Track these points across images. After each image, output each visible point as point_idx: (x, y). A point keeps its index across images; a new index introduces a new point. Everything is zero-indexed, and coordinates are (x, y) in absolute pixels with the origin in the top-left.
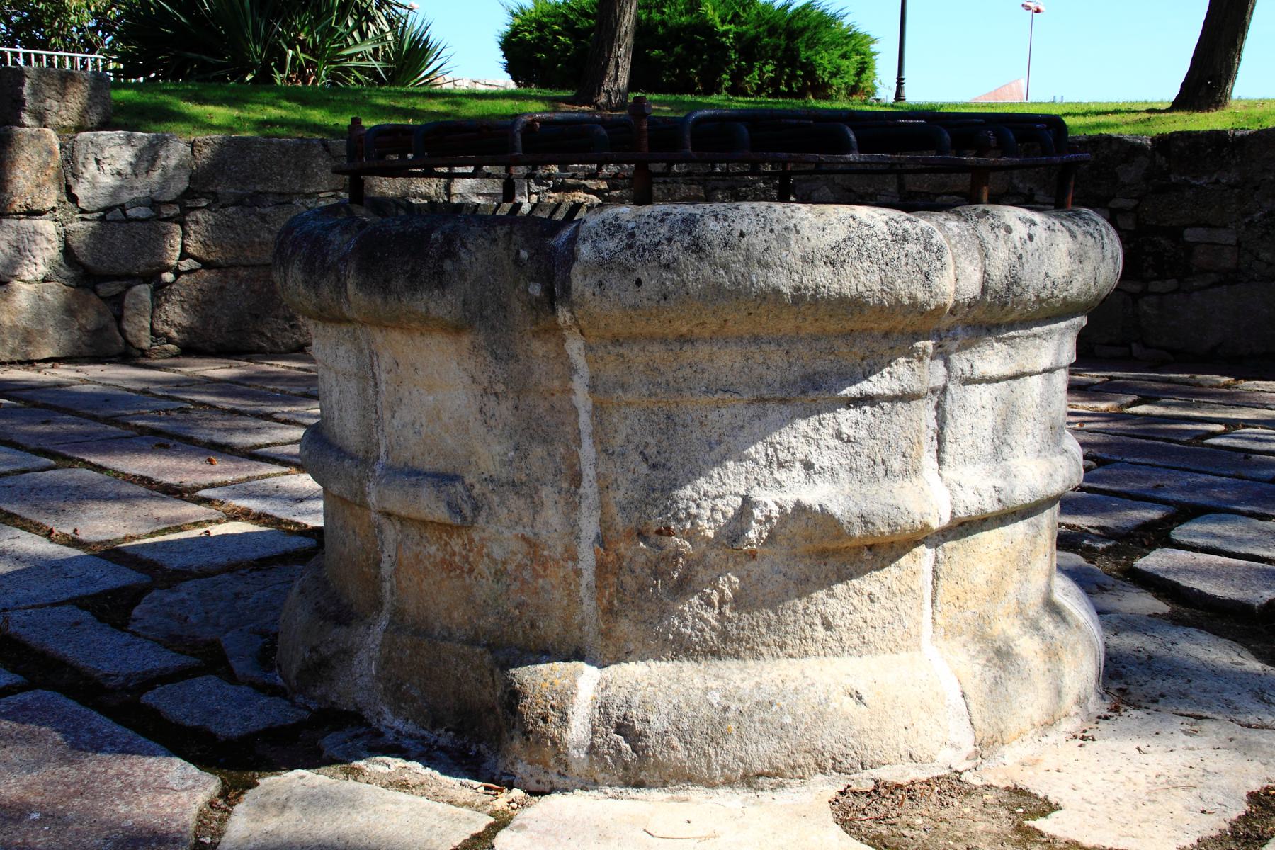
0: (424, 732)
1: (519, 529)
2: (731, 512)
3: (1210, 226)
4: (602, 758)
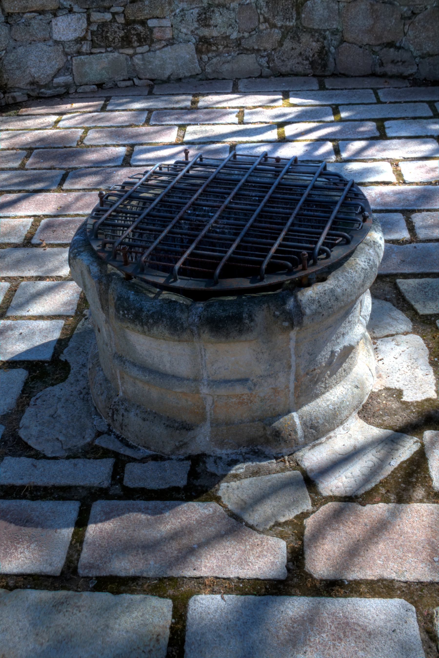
0: (235, 451)
1: (271, 387)
2: (329, 356)
3: (158, 18)
4: (309, 438)
